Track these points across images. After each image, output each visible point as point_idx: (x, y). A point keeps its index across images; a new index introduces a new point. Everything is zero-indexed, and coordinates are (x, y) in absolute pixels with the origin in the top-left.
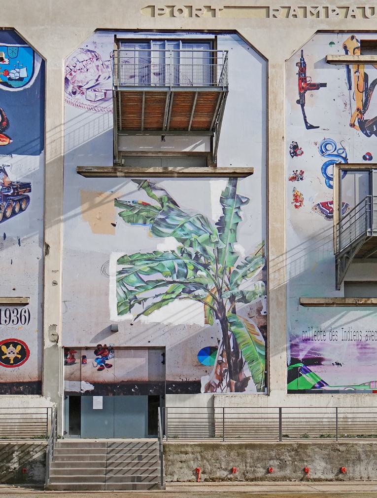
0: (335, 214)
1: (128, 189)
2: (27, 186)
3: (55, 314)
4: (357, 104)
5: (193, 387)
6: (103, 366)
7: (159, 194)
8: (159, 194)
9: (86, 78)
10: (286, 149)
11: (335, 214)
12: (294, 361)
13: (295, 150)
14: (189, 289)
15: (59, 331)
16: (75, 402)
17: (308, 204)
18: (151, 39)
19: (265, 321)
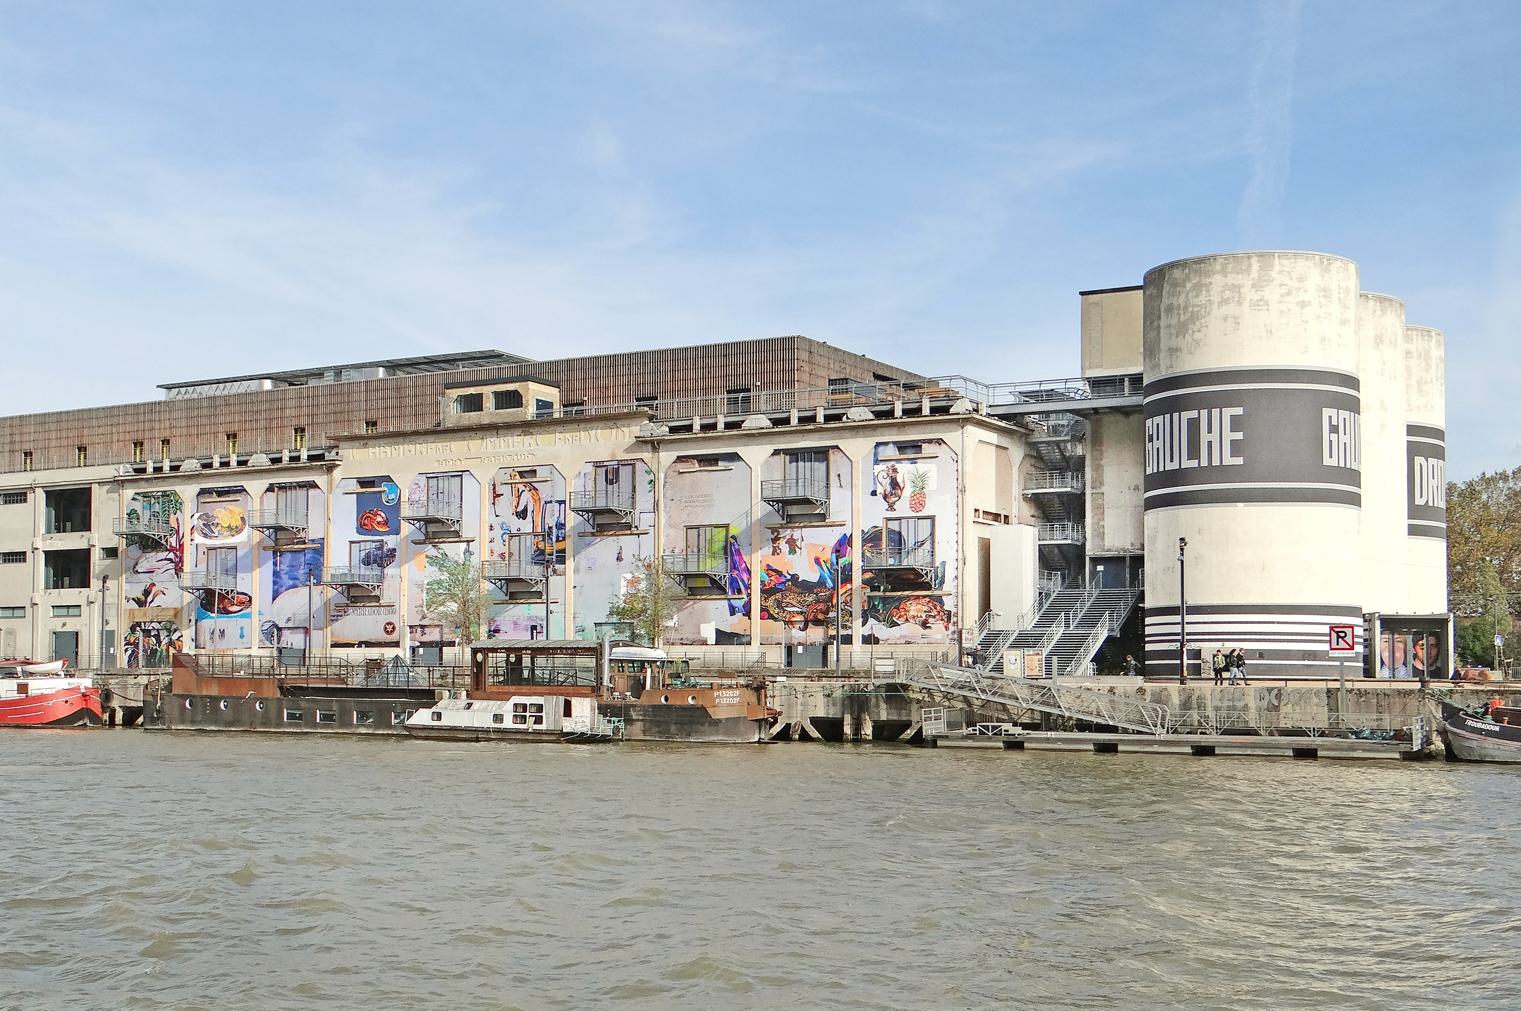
0: (507, 558)
1: (430, 550)
2: (394, 550)
3: (404, 611)
4: (515, 504)
5: (452, 644)
6: (423, 634)
7: (441, 551)
8: (441, 551)
9: (415, 497)
10: (488, 528)
11: (507, 558)
12: (490, 631)
13: (491, 528)
14: (453, 597)
15: (406, 618)
16: (414, 650)
17: (496, 554)
18: (924, 441)
19: (891, 446)
